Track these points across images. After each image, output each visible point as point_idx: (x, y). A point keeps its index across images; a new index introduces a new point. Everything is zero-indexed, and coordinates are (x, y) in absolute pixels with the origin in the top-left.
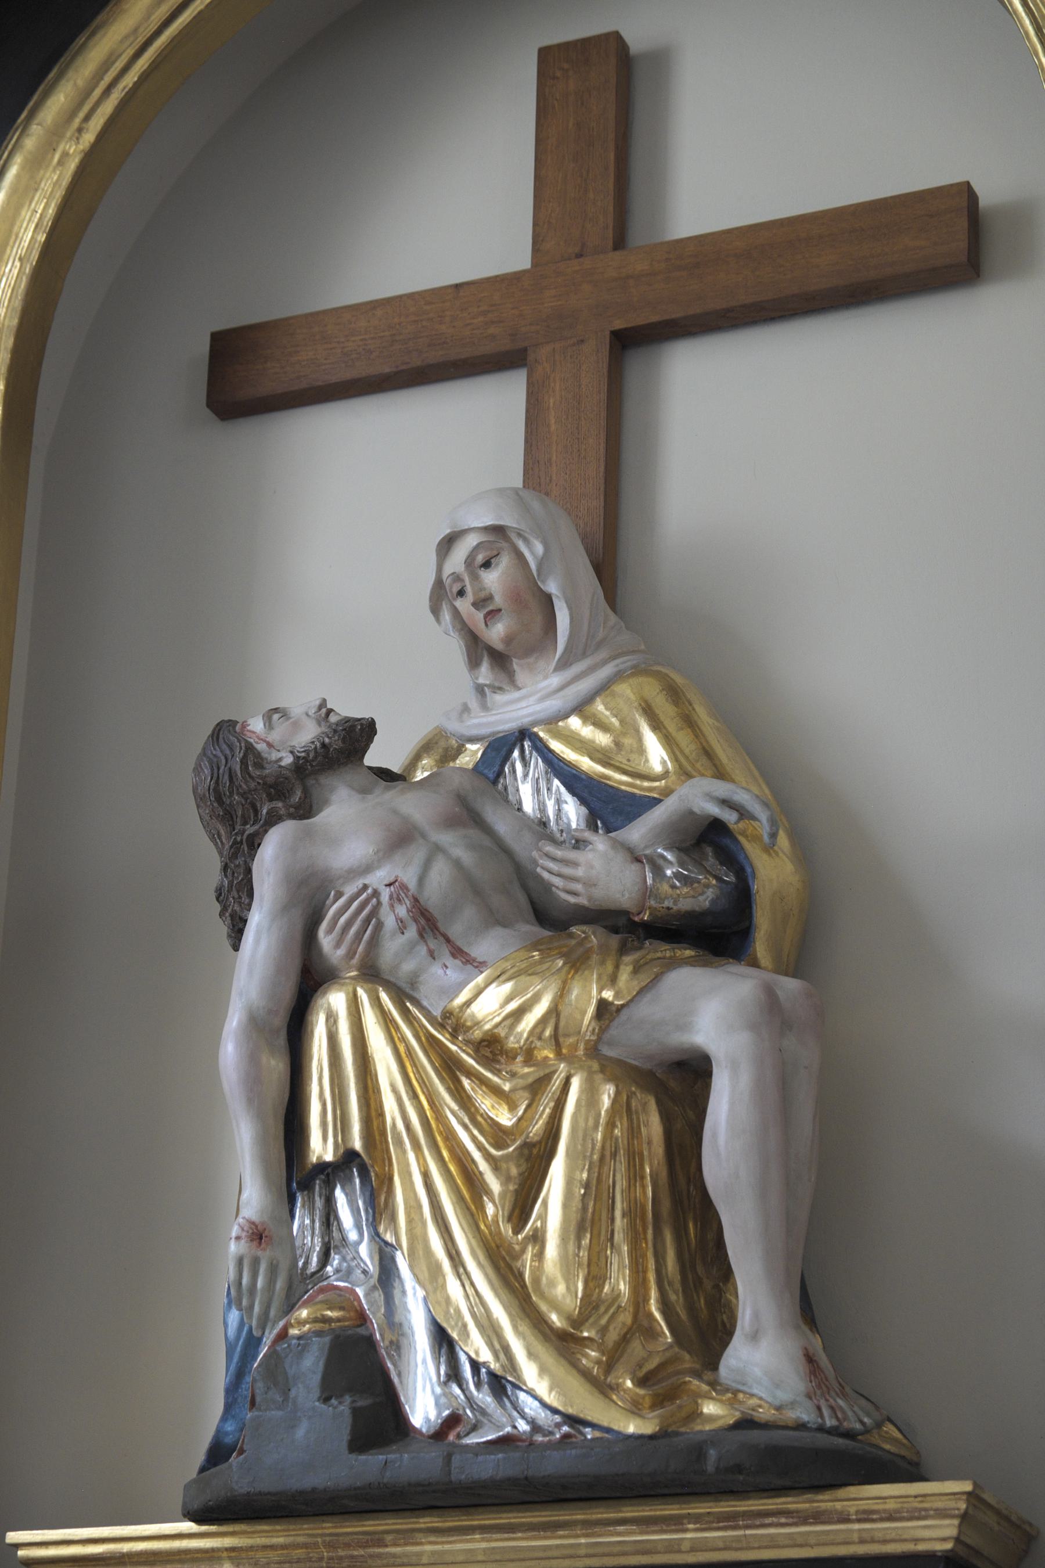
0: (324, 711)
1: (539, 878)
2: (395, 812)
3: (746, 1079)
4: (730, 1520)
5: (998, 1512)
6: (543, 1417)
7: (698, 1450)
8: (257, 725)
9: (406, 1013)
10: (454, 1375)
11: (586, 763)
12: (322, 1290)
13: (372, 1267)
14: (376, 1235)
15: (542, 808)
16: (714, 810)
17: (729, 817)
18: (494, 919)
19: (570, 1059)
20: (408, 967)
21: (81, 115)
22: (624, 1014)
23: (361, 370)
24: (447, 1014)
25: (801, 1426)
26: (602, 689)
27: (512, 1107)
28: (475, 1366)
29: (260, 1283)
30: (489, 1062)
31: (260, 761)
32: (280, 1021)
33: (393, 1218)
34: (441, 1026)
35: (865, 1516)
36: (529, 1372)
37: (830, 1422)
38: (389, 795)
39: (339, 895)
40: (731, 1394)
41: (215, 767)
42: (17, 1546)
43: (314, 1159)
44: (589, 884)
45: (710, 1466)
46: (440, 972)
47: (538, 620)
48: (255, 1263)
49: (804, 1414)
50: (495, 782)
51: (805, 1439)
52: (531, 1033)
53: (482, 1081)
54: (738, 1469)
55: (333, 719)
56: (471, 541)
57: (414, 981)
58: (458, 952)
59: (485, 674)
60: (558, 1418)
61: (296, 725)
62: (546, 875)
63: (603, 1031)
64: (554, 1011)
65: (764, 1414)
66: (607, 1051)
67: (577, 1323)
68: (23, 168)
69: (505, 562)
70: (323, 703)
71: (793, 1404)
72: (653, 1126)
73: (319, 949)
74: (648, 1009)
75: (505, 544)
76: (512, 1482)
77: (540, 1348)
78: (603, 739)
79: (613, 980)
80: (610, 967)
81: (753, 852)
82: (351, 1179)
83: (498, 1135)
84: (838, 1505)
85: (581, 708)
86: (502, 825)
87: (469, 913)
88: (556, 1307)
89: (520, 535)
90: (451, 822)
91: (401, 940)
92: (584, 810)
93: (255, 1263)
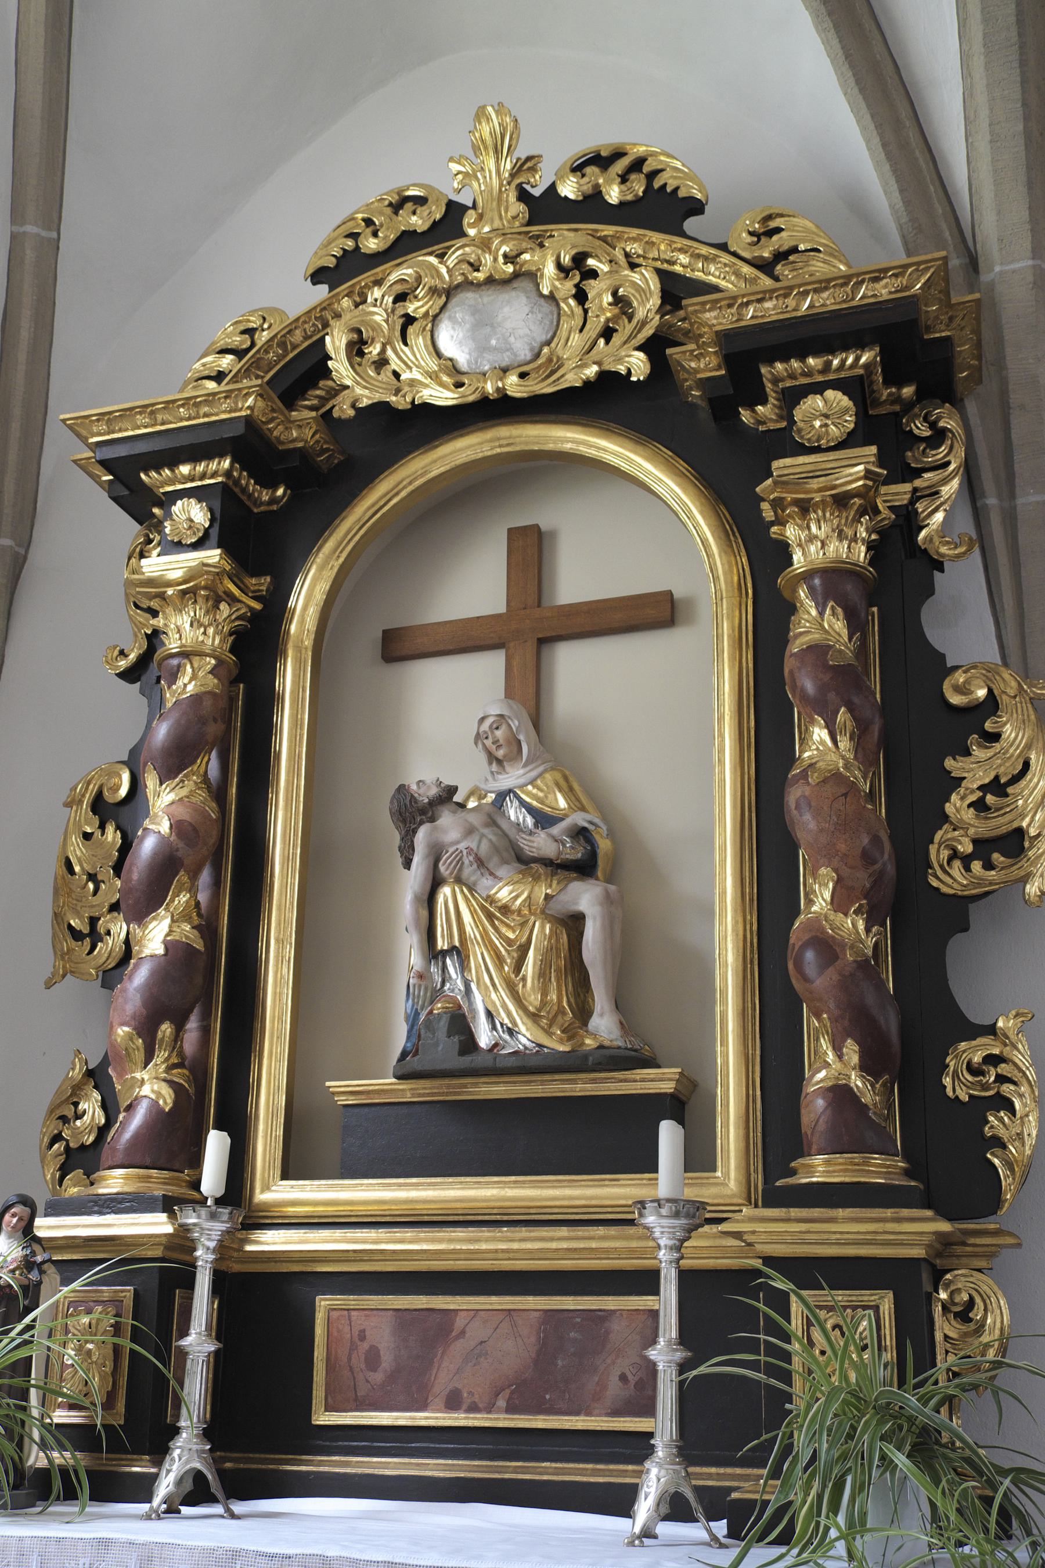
0: (439, 783)
1: (519, 846)
2: (466, 821)
3: (598, 923)
4: (594, 1081)
5: (687, 1078)
6: (528, 1044)
7: (586, 1056)
8: (414, 787)
9: (473, 895)
10: (494, 1028)
11: (535, 803)
12: (444, 996)
13: (462, 988)
14: (463, 976)
15: (518, 819)
16: (586, 825)
17: (591, 827)
18: (504, 862)
19: (534, 914)
20: (473, 879)
21: (339, 550)
22: (554, 899)
23: (441, 647)
24: (488, 896)
25: (619, 1048)
26: (540, 775)
27: (514, 932)
28: (502, 1025)
29: (422, 993)
30: (504, 914)
31: (416, 801)
32: (426, 897)
33: (470, 971)
34: (486, 901)
35: (643, 1080)
36: (523, 1028)
37: (629, 1046)
38: (463, 814)
39: (447, 852)
40: (594, 1036)
41: (399, 802)
42: (330, 1087)
43: (439, 948)
44: (538, 849)
45: (590, 1063)
46: (485, 881)
47: (515, 748)
48: (420, 986)
49: (620, 1043)
50: (500, 809)
51: (622, 1052)
52: (520, 904)
53: (502, 922)
54: (600, 1063)
55: (442, 785)
56: (491, 720)
57: (475, 884)
58: (491, 874)
59: (495, 767)
60: (534, 1045)
61: (429, 787)
62: (522, 845)
63: (546, 904)
64: (529, 897)
65: (607, 1043)
66: (547, 912)
67: (539, 1010)
68: (317, 570)
69: (504, 727)
70: (438, 780)
71: (616, 1040)
72: (564, 939)
73: (439, 871)
74: (563, 897)
75: (503, 721)
76: (519, 1068)
77: (525, 1019)
78: (541, 794)
79: (551, 886)
80: (549, 880)
81: (597, 837)
82: (453, 955)
83: (509, 942)
84: (633, 1076)
85: (532, 782)
86: (504, 825)
87: (496, 859)
88: (531, 1004)
89: (509, 718)
90: (487, 825)
91: (471, 869)
92: (534, 820)
93: (420, 986)
